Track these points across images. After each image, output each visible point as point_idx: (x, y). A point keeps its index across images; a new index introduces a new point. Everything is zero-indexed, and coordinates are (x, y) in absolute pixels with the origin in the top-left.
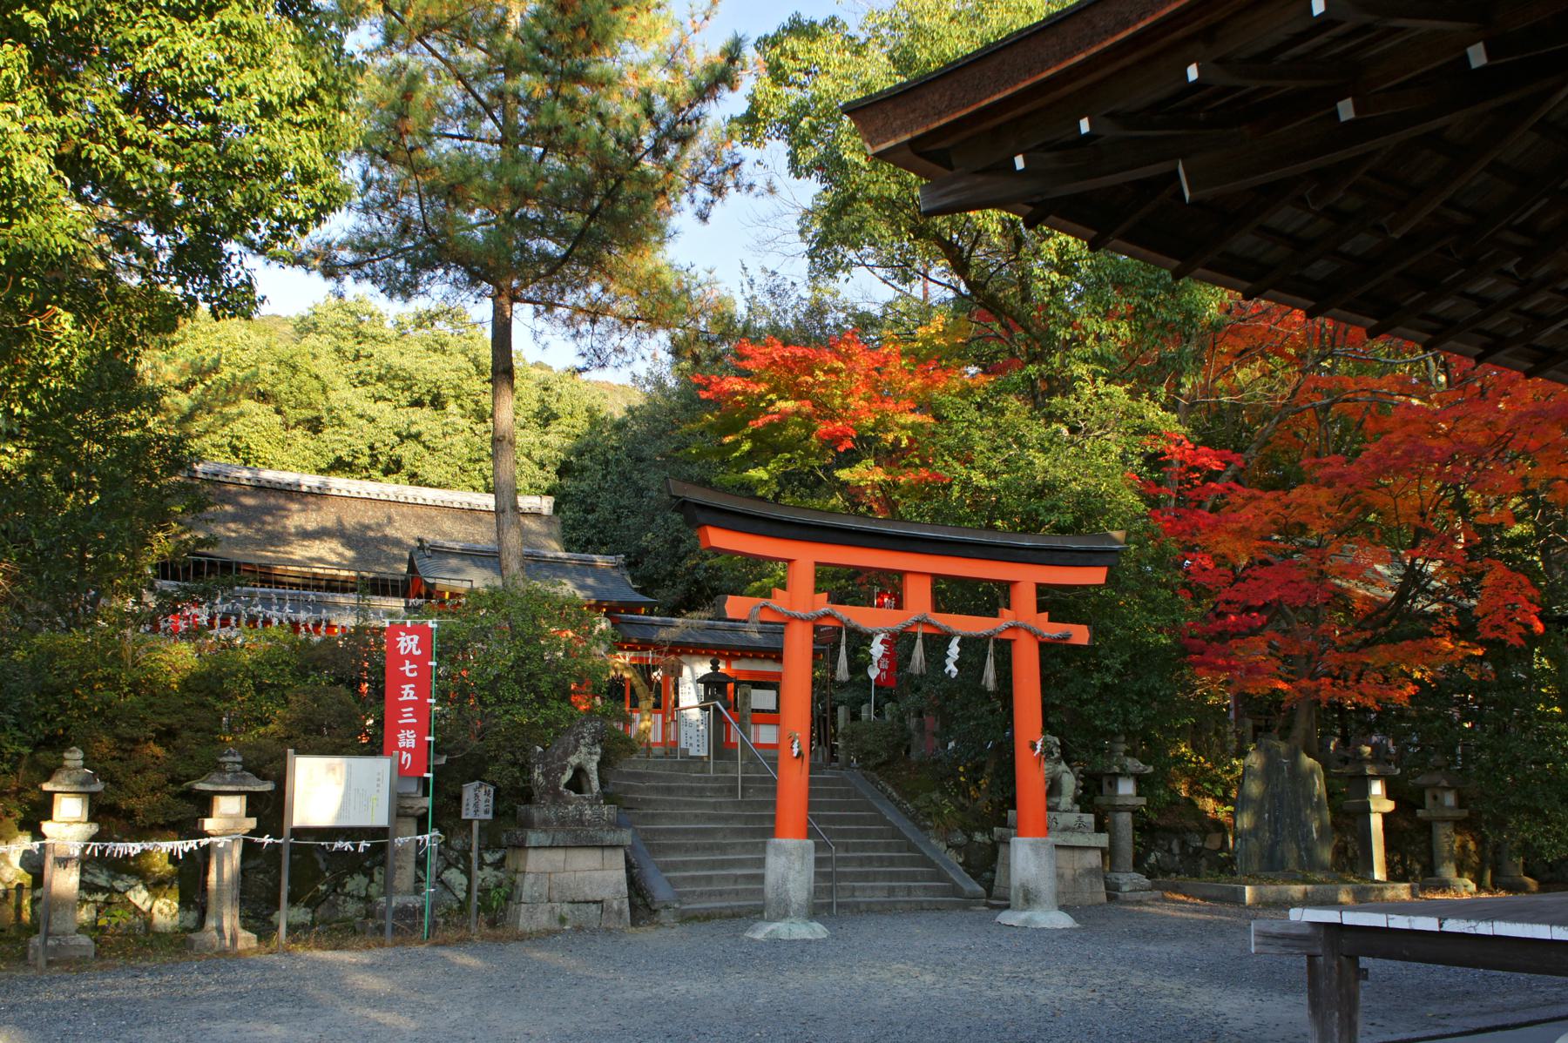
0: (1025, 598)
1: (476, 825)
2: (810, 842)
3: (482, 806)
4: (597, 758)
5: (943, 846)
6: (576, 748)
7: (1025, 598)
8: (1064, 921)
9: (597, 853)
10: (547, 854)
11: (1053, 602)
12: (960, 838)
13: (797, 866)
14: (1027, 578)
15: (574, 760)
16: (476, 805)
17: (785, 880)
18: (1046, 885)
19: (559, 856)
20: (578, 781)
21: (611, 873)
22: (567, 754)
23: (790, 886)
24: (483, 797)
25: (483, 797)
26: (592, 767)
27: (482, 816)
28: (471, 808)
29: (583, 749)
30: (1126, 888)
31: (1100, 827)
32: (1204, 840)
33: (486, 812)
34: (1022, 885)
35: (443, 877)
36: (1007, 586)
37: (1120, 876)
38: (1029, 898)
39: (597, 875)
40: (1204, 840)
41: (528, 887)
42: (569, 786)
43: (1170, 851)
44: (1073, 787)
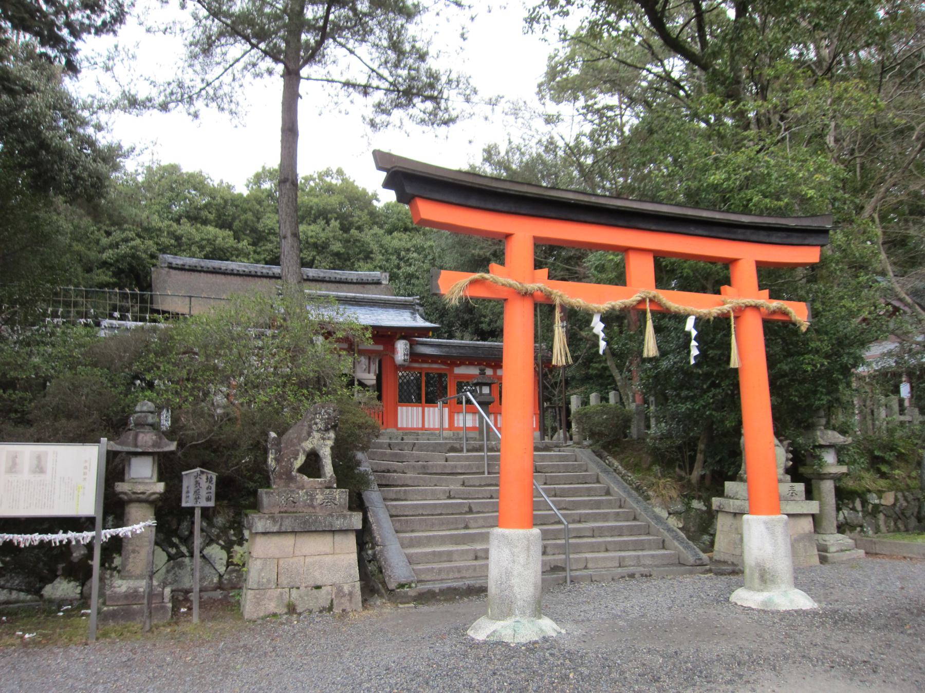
0: (745, 274)
1: (198, 513)
2: (536, 531)
3: (203, 493)
4: (330, 443)
5: (665, 514)
6: (309, 434)
7: (745, 274)
8: (802, 601)
9: (328, 539)
10: (276, 540)
11: (772, 278)
12: (679, 507)
13: (522, 559)
14: (747, 256)
15: (308, 445)
16: (197, 492)
17: (508, 574)
18: (783, 565)
19: (287, 542)
20: (312, 466)
21: (342, 557)
22: (301, 440)
23: (515, 581)
24: (204, 483)
25: (204, 483)
26: (326, 453)
27: (204, 503)
28: (191, 494)
29: (316, 435)
30: (832, 549)
31: (809, 495)
32: (880, 498)
33: (208, 499)
34: (758, 565)
35: (205, 552)
36: (729, 263)
37: (826, 537)
38: (766, 578)
39: (328, 559)
40: (880, 498)
41: (255, 572)
42: (301, 470)
43: (854, 509)
44: (784, 459)
